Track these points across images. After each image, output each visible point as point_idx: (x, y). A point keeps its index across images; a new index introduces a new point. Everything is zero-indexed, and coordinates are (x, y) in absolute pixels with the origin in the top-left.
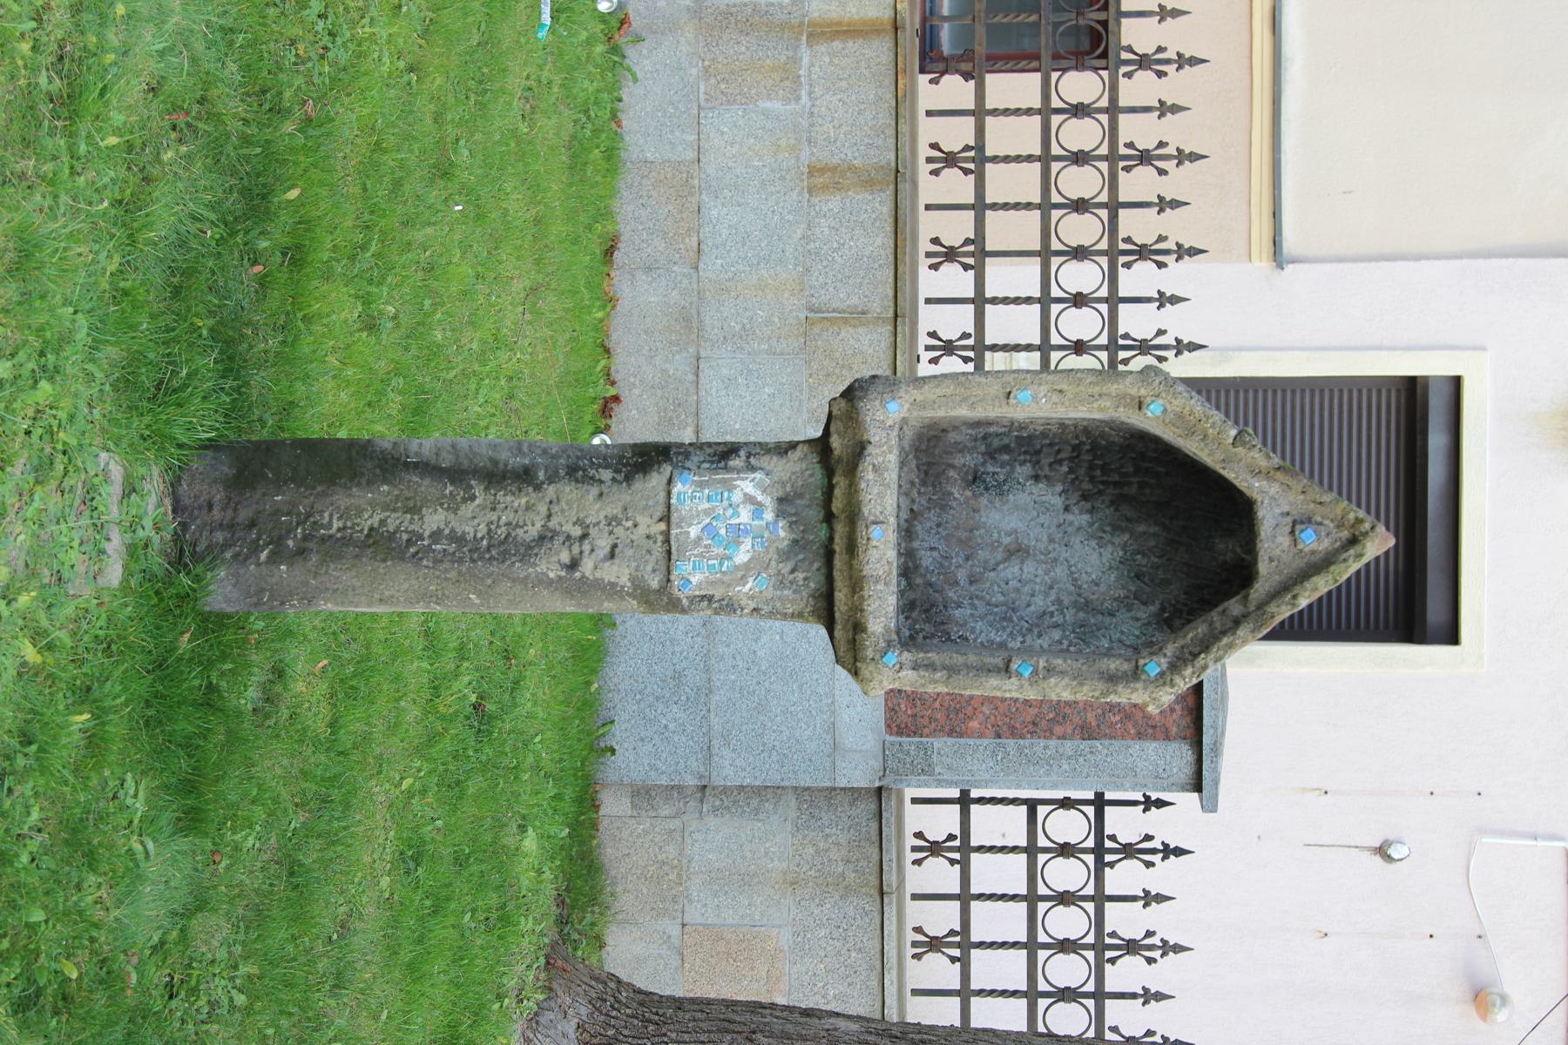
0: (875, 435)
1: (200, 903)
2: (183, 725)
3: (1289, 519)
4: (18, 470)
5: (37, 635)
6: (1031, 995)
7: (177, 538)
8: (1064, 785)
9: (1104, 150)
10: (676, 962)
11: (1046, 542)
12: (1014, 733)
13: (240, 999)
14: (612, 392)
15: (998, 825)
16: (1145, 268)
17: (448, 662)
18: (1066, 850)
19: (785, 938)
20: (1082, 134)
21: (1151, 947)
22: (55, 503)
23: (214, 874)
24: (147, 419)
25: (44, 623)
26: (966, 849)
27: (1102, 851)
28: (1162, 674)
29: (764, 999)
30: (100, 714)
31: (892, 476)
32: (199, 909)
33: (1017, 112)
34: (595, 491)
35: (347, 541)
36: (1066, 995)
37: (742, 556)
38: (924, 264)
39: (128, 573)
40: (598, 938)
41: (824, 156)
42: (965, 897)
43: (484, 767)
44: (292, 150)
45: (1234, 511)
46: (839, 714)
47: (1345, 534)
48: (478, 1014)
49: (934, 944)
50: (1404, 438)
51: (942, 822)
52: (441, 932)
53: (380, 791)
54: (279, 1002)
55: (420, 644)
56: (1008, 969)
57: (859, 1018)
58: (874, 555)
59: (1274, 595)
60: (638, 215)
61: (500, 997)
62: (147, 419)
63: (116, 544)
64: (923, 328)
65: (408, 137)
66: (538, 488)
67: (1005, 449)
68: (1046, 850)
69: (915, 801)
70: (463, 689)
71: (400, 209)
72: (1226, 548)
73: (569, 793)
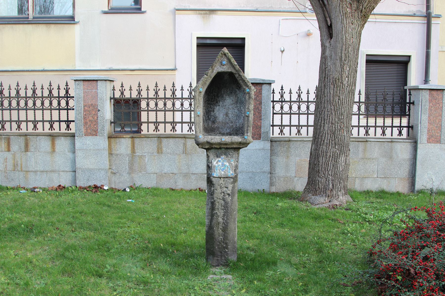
0: (205, 140)
1: (289, 262)
2: (257, 265)
3: (221, 65)
4: (211, 293)
5: (240, 290)
6: (308, 114)
7: (223, 266)
8: (270, 108)
9: (155, 100)
10: (302, 178)
11: (225, 110)
12: (261, 117)
13: (307, 255)
14: (198, 189)
15: (277, 120)
16: (176, 93)
17: (247, 219)
18: (282, 108)
19: (297, 159)
20: (152, 104)
21: (299, 92)
22: (217, 286)
23: (284, 260)
24: (202, 271)
25: (238, 288)
26: (281, 126)
27: (282, 101)
28: (249, 89)
29: (308, 162)
30: (255, 279)
31: (213, 137)
32: (290, 262)
33: (148, 116)
34: (215, 191)
35: (224, 235)
36: (308, 108)
37: (227, 164)
38: (175, 133)
39: (230, 274)
40: (297, 192)
41: (156, 151)
42: (290, 126)
43: (266, 212)
44: (154, 245)
45: (219, 75)
46: (255, 149)
47: (224, 56)
48: (310, 213)
49: (299, 131)
50: (207, 47)
51: (277, 130)
52: (296, 220)
53: (270, 231)
54: (307, 248)
55: (243, 224)
56: (303, 118)
57: (312, 145)
58: (227, 140)
59: (235, 68)
60: (166, 185)
61: (308, 210)
62: (202, 271)
63: (224, 276)
64: (187, 133)
65: (152, 225)
66: (215, 201)
67: (208, 117)
68: (282, 111)
69: (273, 135)
70: (252, 216)
71: (165, 226)
72: (226, 77)
73: (271, 197)
